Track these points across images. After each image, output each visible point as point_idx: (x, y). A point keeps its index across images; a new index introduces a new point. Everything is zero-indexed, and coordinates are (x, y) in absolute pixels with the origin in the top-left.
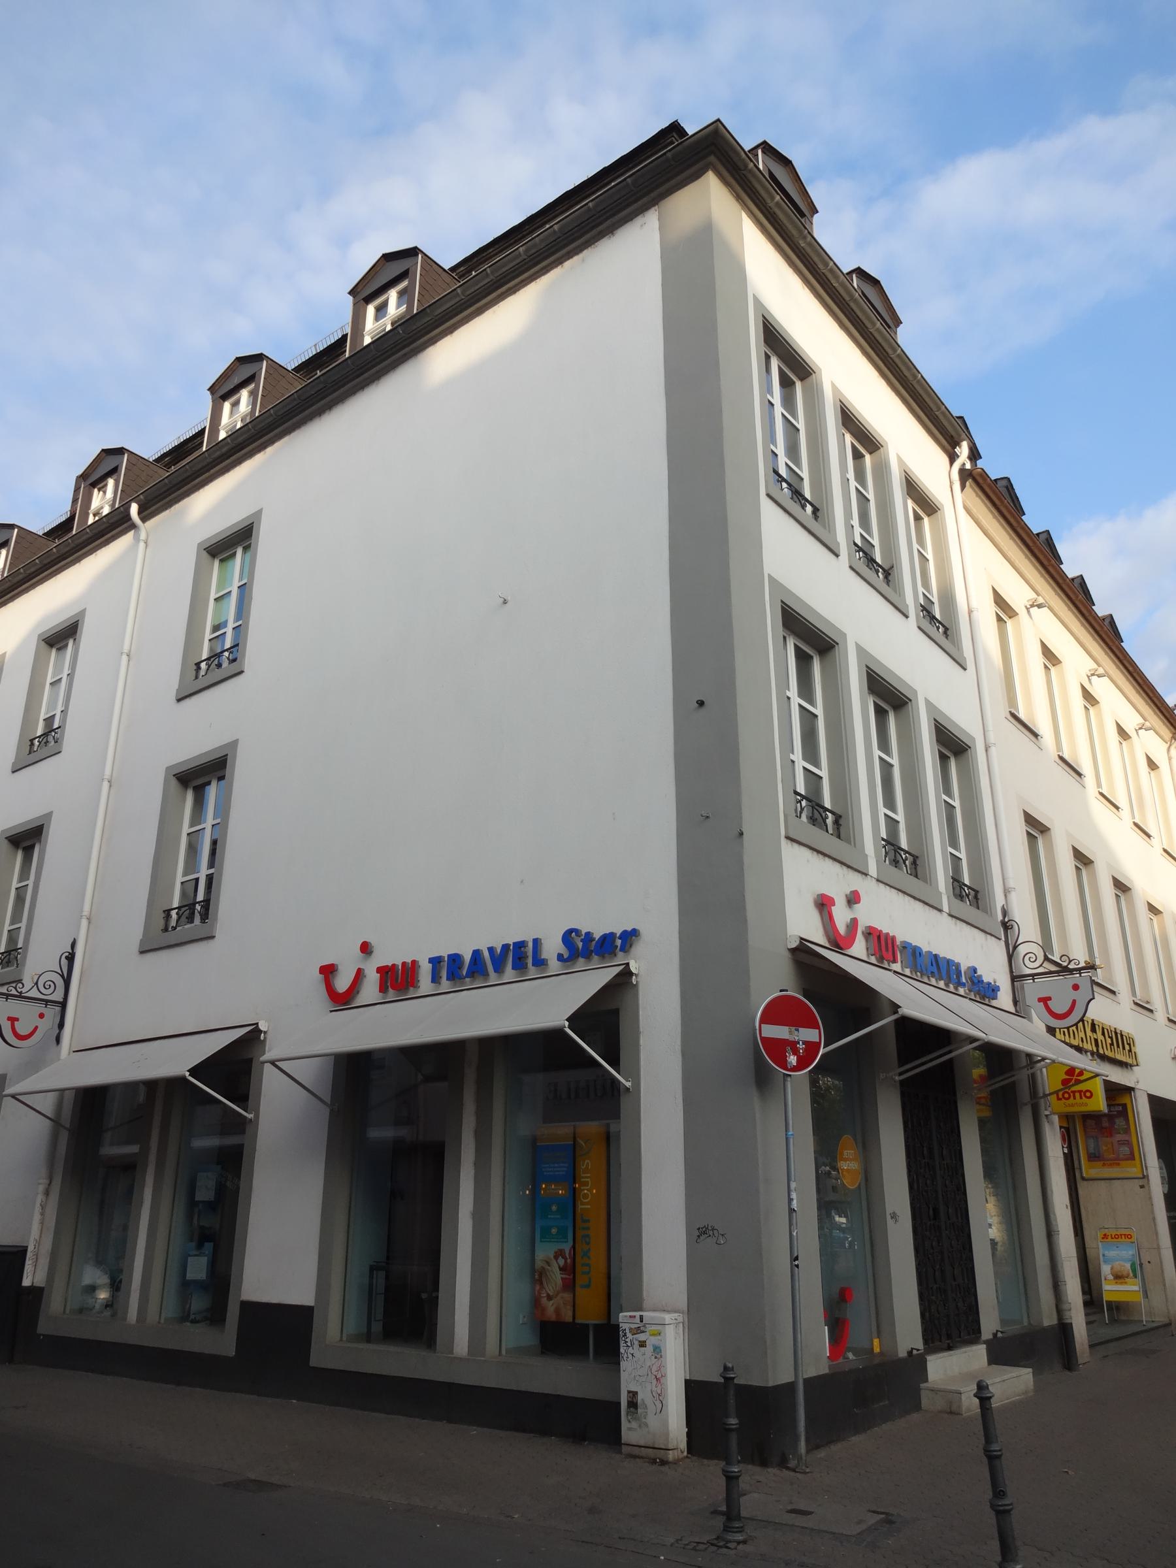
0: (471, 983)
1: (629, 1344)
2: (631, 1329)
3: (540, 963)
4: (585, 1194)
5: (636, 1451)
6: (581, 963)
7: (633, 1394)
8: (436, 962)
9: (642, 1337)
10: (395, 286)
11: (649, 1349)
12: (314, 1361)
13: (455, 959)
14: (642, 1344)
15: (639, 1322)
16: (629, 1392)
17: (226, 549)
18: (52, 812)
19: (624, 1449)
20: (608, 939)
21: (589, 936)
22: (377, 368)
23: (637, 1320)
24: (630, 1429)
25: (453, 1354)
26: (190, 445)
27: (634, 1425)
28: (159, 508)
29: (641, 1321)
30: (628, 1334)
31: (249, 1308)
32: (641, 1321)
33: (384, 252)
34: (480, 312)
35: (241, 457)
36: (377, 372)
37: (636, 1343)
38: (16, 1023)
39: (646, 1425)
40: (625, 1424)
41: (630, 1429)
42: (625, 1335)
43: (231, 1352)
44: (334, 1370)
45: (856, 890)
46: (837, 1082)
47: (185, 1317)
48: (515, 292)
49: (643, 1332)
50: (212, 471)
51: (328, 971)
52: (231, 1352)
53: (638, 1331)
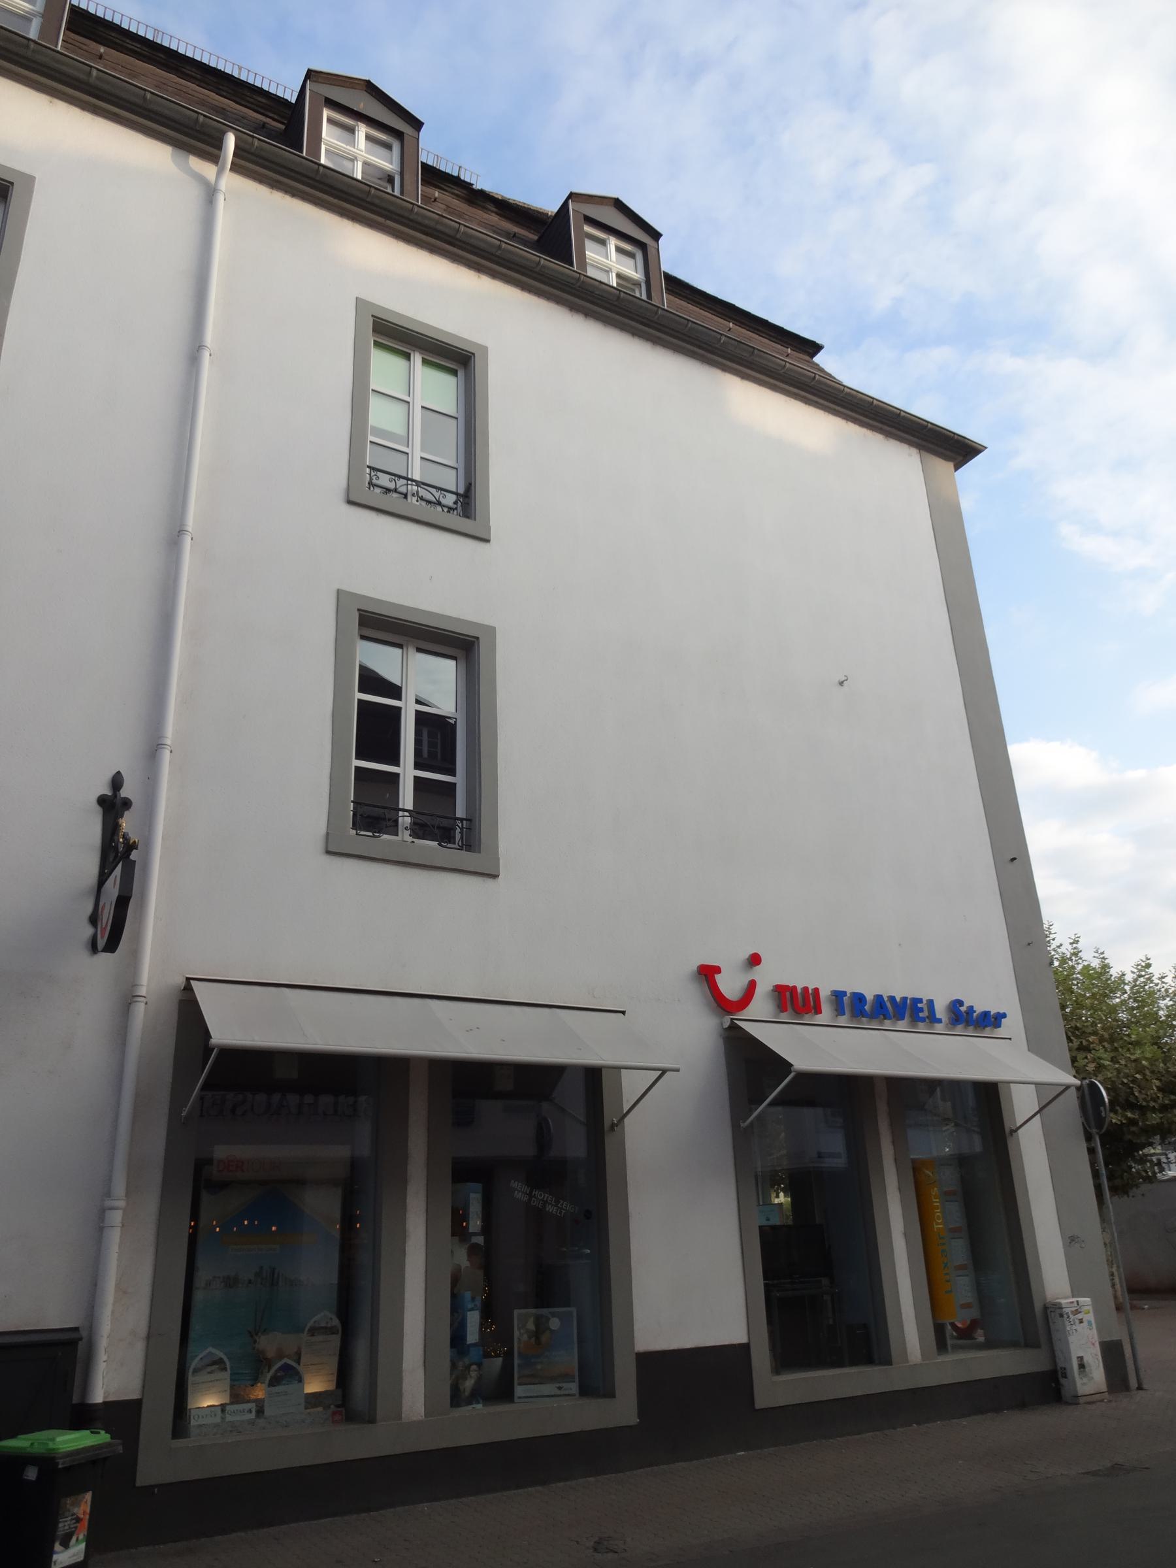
0: (869, 1023)
1: (1072, 1323)
2: (1072, 1312)
3: (933, 1019)
4: (938, 1216)
5: (1089, 1399)
6: (959, 1029)
7: (1081, 1358)
8: (838, 996)
9: (1080, 1316)
10: (619, 239)
11: (1085, 1324)
12: (760, 1403)
13: (859, 998)
14: (1081, 1321)
15: (1076, 1305)
16: (1078, 1357)
17: (430, 352)
18: (119, 773)
19: (1082, 1400)
20: (986, 1014)
21: (971, 1009)
22: (663, 336)
23: (1075, 1304)
24: (1084, 1384)
25: (908, 1362)
26: (188, 68)
27: (1085, 1380)
28: (256, 172)
29: (1078, 1305)
30: (1071, 1316)
31: (651, 1363)
32: (1078, 1305)
33: (621, 199)
34: (807, 401)
35: (439, 249)
36: (659, 338)
37: (1077, 1321)
38: (718, 977)
39: (1092, 1378)
40: (1079, 1382)
41: (1084, 1384)
42: (1069, 1317)
43: (632, 1419)
44: (885, 1392)
45: (882, 995)
46: (1139, 1141)
47: (457, 1398)
48: (806, 403)
49: (1080, 1312)
50: (389, 223)
51: (708, 973)
52: (632, 1419)
53: (1077, 1312)
